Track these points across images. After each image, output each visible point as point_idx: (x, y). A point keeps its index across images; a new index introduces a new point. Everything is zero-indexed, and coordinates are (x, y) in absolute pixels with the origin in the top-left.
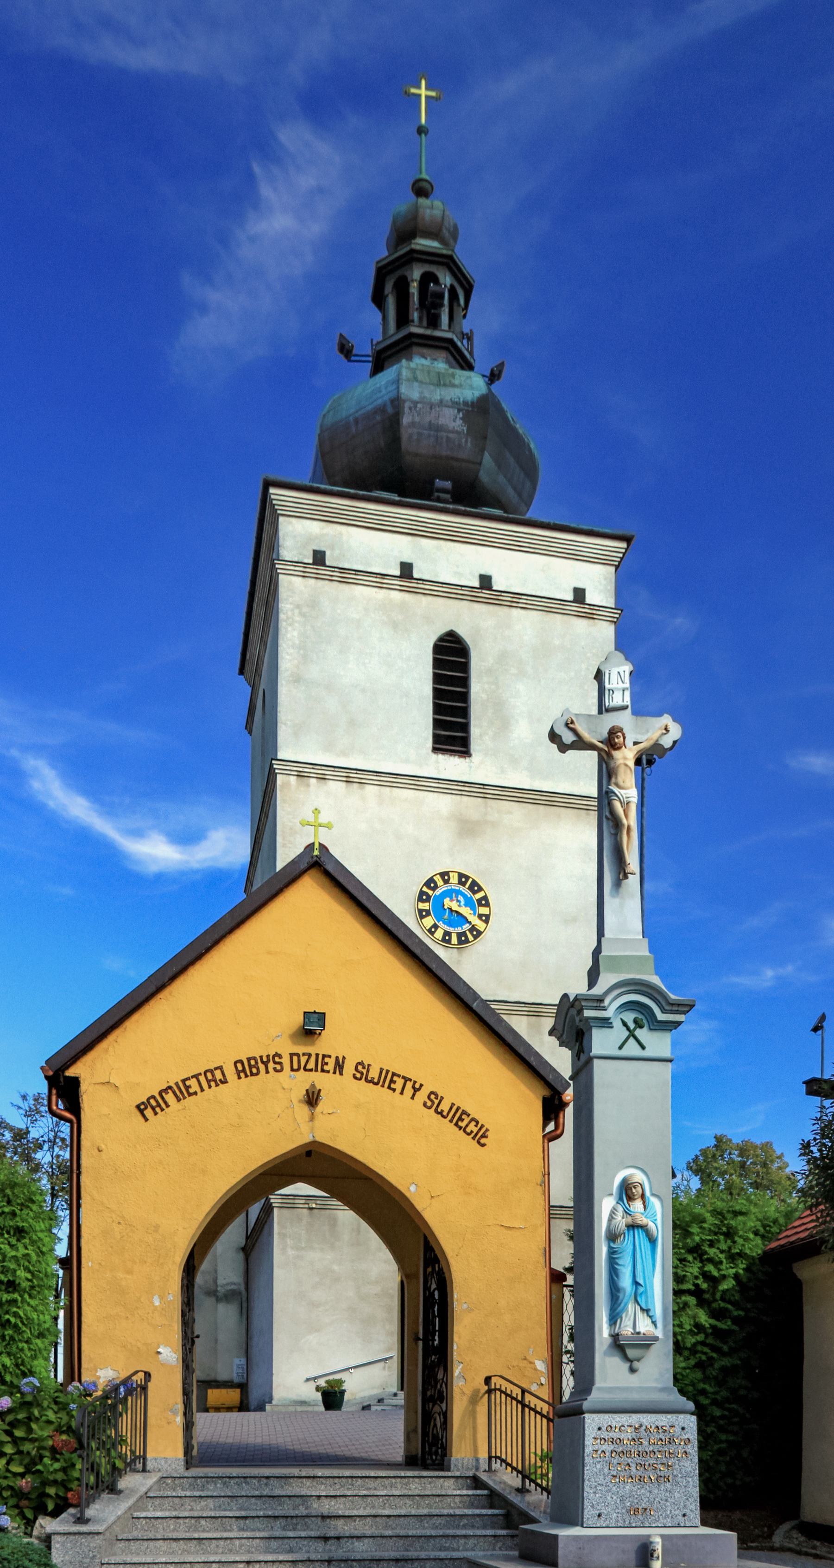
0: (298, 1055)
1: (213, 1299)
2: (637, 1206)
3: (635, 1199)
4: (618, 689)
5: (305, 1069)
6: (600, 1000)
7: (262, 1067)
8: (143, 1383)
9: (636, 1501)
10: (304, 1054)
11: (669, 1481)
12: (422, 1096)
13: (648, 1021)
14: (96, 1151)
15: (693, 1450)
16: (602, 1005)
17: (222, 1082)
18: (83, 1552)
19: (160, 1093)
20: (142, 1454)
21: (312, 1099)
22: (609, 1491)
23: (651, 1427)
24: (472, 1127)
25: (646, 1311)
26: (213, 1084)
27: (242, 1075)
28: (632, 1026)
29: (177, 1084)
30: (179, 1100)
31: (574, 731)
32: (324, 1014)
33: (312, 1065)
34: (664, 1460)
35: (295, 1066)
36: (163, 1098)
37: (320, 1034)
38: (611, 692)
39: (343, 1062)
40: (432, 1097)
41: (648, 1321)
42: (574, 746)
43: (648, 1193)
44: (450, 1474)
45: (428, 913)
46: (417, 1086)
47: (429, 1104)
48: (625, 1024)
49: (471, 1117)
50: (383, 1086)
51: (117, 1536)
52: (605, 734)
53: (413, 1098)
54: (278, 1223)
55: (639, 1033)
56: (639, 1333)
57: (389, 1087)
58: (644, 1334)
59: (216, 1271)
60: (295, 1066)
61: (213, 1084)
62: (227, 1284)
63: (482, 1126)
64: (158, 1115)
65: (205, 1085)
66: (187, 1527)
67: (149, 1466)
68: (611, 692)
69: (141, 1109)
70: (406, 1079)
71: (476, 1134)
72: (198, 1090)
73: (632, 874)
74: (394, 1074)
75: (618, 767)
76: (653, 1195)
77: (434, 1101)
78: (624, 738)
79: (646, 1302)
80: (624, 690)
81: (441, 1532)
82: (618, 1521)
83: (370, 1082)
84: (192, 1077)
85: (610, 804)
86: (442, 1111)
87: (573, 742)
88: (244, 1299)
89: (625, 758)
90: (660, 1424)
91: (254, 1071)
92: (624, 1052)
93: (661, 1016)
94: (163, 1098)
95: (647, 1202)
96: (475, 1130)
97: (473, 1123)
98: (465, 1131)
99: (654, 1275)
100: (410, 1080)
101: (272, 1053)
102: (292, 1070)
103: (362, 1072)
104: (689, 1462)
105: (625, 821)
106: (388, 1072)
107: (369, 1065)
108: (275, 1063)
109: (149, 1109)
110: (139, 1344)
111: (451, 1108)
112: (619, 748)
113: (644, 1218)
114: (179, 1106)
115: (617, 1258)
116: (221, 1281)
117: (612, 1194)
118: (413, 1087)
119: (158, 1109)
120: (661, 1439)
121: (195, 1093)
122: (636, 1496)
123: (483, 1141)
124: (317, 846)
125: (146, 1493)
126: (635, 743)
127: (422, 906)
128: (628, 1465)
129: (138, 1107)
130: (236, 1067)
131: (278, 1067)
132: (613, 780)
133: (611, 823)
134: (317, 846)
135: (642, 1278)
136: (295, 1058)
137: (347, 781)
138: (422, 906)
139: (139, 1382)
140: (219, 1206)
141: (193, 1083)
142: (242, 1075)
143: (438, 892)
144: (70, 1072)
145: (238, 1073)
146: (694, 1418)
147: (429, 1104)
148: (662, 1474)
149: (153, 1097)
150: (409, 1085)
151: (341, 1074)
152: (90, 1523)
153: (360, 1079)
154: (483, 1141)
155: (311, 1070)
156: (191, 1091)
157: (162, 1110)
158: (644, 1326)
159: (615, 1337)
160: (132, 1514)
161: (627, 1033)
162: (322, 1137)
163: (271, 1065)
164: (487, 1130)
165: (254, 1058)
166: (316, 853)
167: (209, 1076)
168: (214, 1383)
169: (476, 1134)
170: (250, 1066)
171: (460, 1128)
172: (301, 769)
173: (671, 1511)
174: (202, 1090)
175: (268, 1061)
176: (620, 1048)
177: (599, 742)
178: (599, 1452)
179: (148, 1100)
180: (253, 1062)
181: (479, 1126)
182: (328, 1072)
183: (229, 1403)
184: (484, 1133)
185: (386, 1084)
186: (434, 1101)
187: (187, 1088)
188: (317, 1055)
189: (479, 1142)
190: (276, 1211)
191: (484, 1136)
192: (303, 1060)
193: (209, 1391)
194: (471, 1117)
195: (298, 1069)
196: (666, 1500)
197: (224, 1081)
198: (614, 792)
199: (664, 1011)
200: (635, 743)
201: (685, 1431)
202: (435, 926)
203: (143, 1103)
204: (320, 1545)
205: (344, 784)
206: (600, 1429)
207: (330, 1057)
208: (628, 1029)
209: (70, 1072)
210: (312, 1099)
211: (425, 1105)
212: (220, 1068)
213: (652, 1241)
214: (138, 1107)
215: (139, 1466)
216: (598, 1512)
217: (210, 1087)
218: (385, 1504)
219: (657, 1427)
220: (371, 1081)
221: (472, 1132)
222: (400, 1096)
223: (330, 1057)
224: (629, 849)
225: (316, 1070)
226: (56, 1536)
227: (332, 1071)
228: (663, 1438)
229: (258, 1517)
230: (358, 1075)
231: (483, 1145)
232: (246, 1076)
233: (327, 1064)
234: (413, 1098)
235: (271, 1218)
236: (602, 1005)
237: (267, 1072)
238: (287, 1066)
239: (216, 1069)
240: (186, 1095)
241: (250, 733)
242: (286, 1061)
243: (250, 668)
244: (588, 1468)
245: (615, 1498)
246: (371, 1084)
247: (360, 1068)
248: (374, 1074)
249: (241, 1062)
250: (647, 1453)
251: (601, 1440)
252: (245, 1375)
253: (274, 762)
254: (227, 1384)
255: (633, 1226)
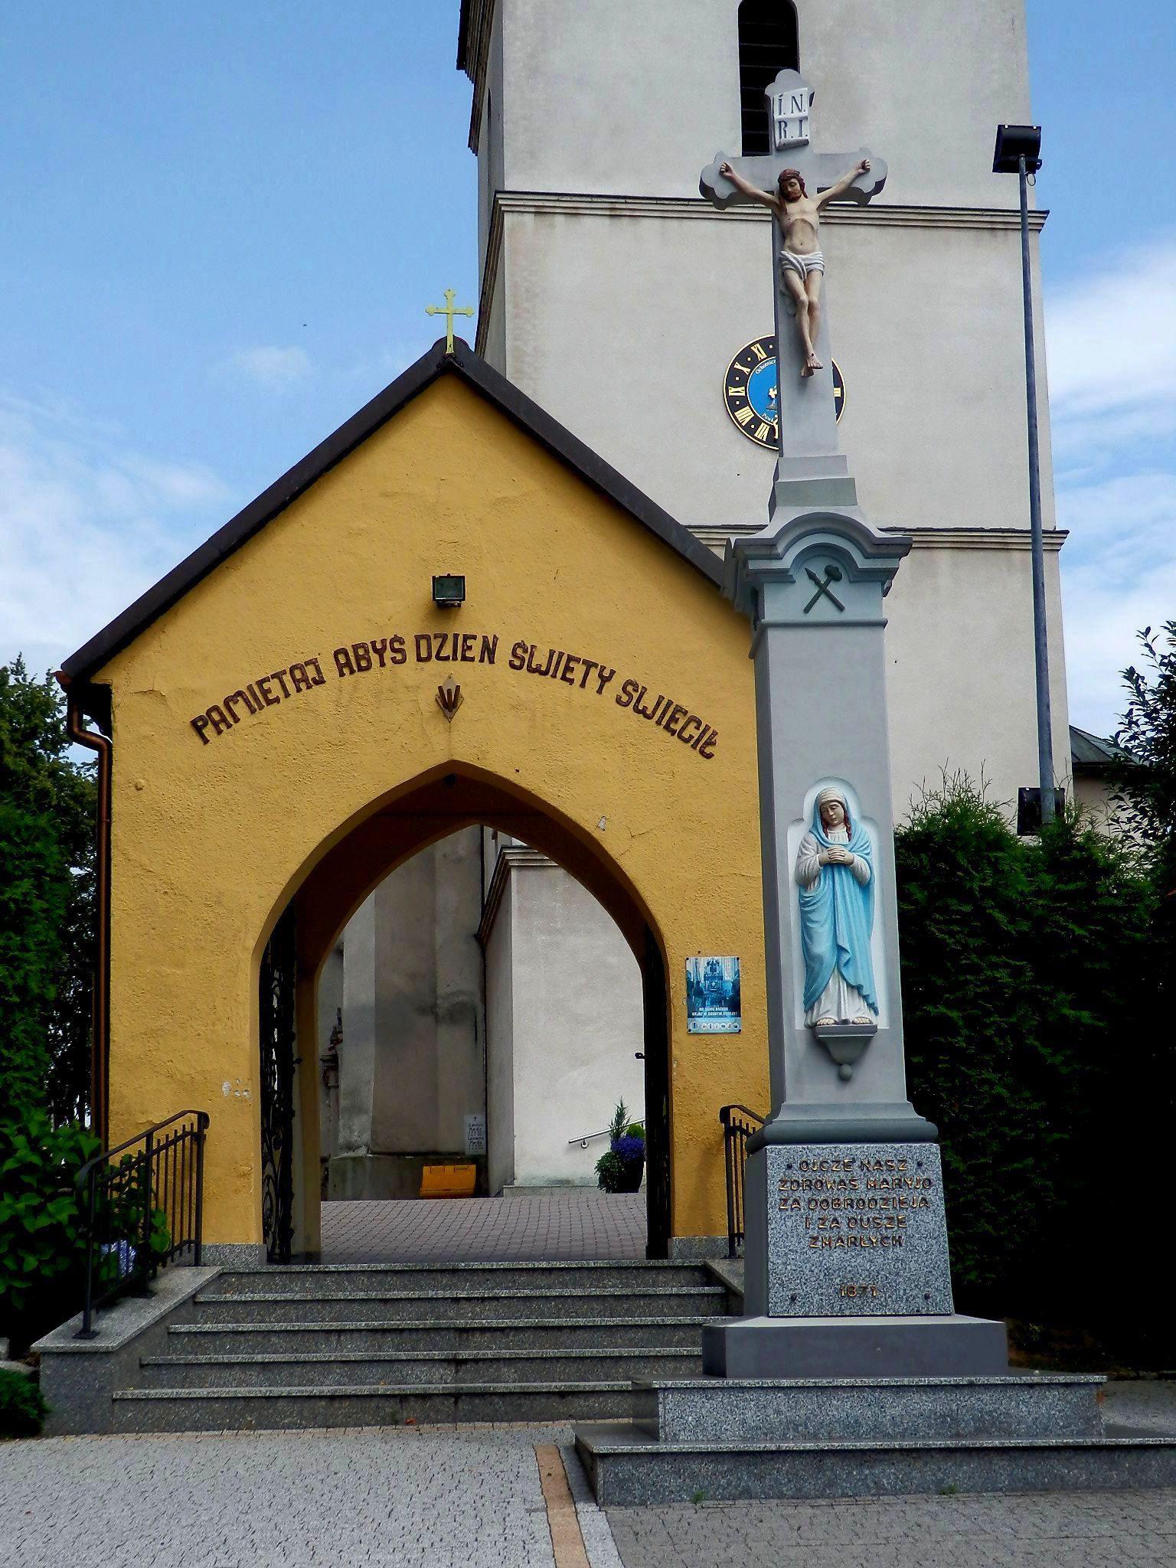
0: (427, 638)
1: (430, 1019)
2: (839, 834)
3: (836, 825)
4: (793, 120)
5: (438, 658)
6: (771, 544)
7: (374, 658)
8: (195, 1130)
9: (849, 1276)
10: (436, 636)
11: (900, 1245)
12: (614, 688)
13: (845, 569)
14: (133, 789)
15: (936, 1196)
16: (774, 552)
17: (317, 683)
18: (86, 1381)
19: (226, 703)
20: (193, 1237)
21: (449, 702)
22: (808, 1260)
23: (869, 1163)
24: (691, 731)
25: (856, 989)
26: (303, 685)
27: (346, 671)
28: (823, 579)
29: (250, 688)
30: (253, 711)
31: (732, 181)
32: (463, 577)
33: (447, 651)
34: (892, 1213)
35: (424, 655)
36: (230, 710)
37: (459, 605)
38: (783, 124)
39: (495, 644)
40: (630, 688)
41: (861, 1004)
42: (730, 201)
43: (854, 815)
44: (665, 1262)
45: (744, 402)
46: (606, 673)
47: (625, 698)
48: (812, 576)
49: (689, 715)
50: (554, 676)
51: (140, 1360)
52: (775, 185)
53: (599, 691)
54: (518, 892)
55: (832, 588)
56: (845, 1022)
57: (564, 678)
58: (853, 1023)
59: (433, 974)
60: (424, 655)
61: (303, 685)
62: (453, 994)
63: (707, 728)
64: (223, 735)
65: (291, 687)
66: (250, 1346)
67: (206, 1256)
68: (783, 124)
69: (198, 726)
70: (589, 665)
71: (698, 741)
72: (281, 695)
73: (817, 368)
74: (570, 659)
75: (793, 224)
76: (864, 818)
77: (632, 695)
78: (802, 186)
79: (856, 976)
80: (801, 121)
81: (636, 1351)
82: (822, 1307)
83: (534, 671)
84: (273, 677)
85: (784, 275)
86: (645, 708)
87: (731, 196)
88: (480, 1017)
89: (804, 212)
90: (884, 1158)
91: (364, 664)
92: (812, 617)
93: (861, 563)
94: (230, 710)
95: (853, 828)
96: (696, 734)
97: (693, 725)
98: (680, 737)
99: (869, 936)
100: (595, 665)
101: (389, 637)
102: (419, 659)
103: (522, 659)
104: (931, 1215)
105: (804, 297)
106: (561, 655)
107: (533, 647)
108: (394, 650)
109: (210, 726)
110: (192, 1072)
111: (658, 704)
112: (795, 199)
113: (846, 852)
114: (255, 719)
115: (810, 912)
116: (442, 990)
117: (802, 820)
118: (600, 675)
119: (222, 726)
120: (885, 1181)
121: (277, 700)
122: (849, 1268)
123: (708, 750)
124: (450, 341)
125: (194, 1296)
126: (820, 190)
127: (732, 391)
128: (835, 1220)
129: (194, 723)
130: (337, 660)
131: (399, 657)
132: (788, 243)
133: (788, 301)
134: (450, 341)
135: (847, 940)
136: (423, 643)
137: (611, 216)
138: (732, 391)
139: (188, 1129)
140: (313, 864)
141: (274, 686)
142: (346, 671)
143: (759, 369)
144: (98, 679)
145: (340, 667)
146: (935, 1147)
147: (625, 698)
148: (889, 1233)
149: (216, 708)
150: (594, 673)
151: (491, 662)
152: (99, 1337)
153: (520, 668)
154: (708, 750)
155: (447, 658)
156: (270, 697)
157: (229, 726)
158: (855, 1012)
159: (812, 1028)
160: (168, 1328)
161: (815, 590)
162: (465, 754)
163: (388, 654)
164: (715, 733)
165: (363, 646)
166: (450, 350)
167: (298, 674)
168: (432, 1157)
169: (698, 741)
170: (358, 658)
171: (673, 732)
172: (540, 203)
173: (905, 1290)
174: (287, 695)
175: (384, 648)
176: (807, 610)
177: (766, 192)
178: (790, 1202)
179: (209, 712)
180: (361, 652)
181: (702, 729)
182: (472, 659)
183: (457, 1188)
184: (710, 738)
185: (559, 674)
186: (632, 695)
187: (265, 693)
188: (456, 636)
189: (702, 752)
190: (514, 874)
191: (710, 743)
192: (435, 644)
193: (426, 1169)
194: (689, 715)
195: (428, 659)
196: (897, 1274)
197: (320, 681)
198: (788, 259)
199: (867, 556)
200: (820, 190)
201: (923, 1168)
202: (756, 421)
203: (201, 718)
204: (449, 1372)
205: (607, 221)
206: (789, 1167)
207: (474, 637)
208: (817, 583)
209: (98, 679)
210: (449, 702)
211: (618, 701)
212: (313, 662)
213: (864, 885)
214: (194, 723)
215: (190, 1257)
216: (790, 1293)
217: (299, 690)
218: (560, 1309)
219: (878, 1162)
220: (538, 670)
221: (691, 737)
222: (581, 689)
223: (474, 637)
224: (814, 335)
225: (455, 659)
226: (46, 1358)
227: (477, 659)
228: (889, 1179)
229: (359, 1331)
230: (517, 663)
231: (709, 756)
232: (352, 672)
233: (470, 648)
234: (599, 691)
235: (508, 883)
236: (774, 552)
237: (383, 664)
238: (411, 656)
239: (307, 663)
240: (264, 703)
241: (475, 151)
242: (410, 647)
243: (472, 56)
244: (772, 1226)
245: (816, 1271)
246: (537, 674)
247: (519, 652)
248: (540, 659)
249: (345, 652)
250: (864, 1202)
251: (792, 1183)
252: (484, 1142)
253: (498, 196)
254: (455, 1158)
255: (832, 865)
